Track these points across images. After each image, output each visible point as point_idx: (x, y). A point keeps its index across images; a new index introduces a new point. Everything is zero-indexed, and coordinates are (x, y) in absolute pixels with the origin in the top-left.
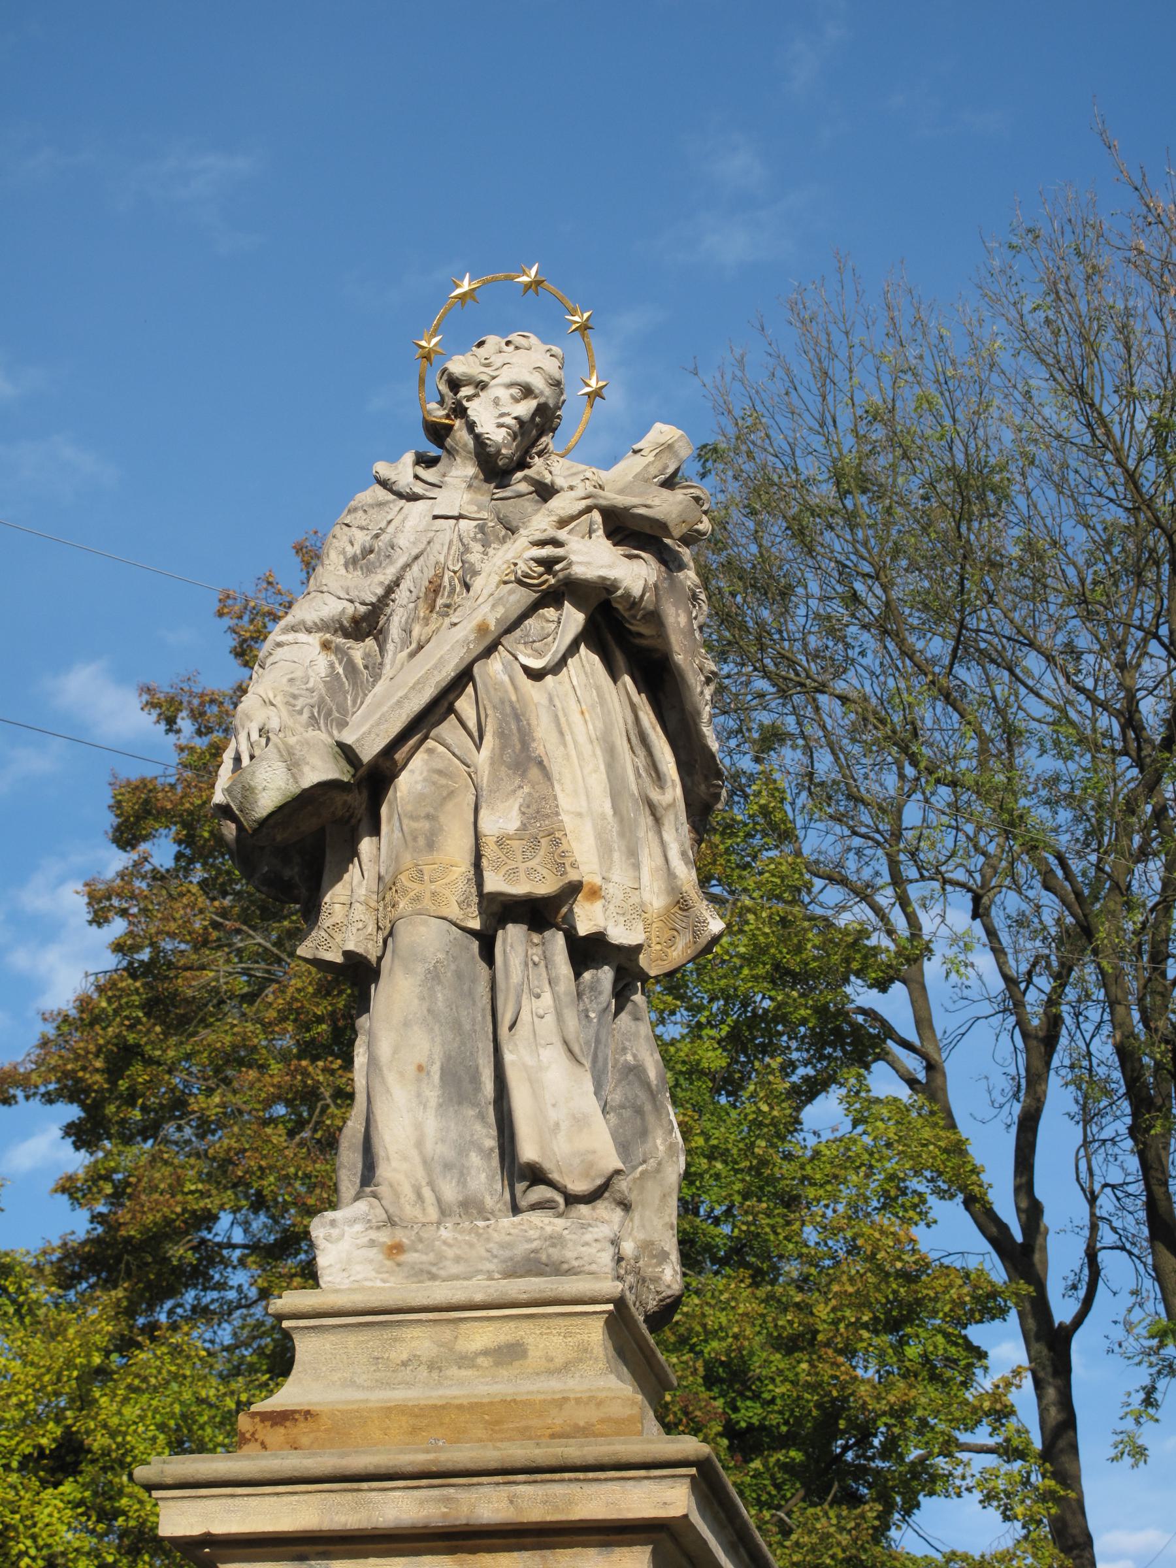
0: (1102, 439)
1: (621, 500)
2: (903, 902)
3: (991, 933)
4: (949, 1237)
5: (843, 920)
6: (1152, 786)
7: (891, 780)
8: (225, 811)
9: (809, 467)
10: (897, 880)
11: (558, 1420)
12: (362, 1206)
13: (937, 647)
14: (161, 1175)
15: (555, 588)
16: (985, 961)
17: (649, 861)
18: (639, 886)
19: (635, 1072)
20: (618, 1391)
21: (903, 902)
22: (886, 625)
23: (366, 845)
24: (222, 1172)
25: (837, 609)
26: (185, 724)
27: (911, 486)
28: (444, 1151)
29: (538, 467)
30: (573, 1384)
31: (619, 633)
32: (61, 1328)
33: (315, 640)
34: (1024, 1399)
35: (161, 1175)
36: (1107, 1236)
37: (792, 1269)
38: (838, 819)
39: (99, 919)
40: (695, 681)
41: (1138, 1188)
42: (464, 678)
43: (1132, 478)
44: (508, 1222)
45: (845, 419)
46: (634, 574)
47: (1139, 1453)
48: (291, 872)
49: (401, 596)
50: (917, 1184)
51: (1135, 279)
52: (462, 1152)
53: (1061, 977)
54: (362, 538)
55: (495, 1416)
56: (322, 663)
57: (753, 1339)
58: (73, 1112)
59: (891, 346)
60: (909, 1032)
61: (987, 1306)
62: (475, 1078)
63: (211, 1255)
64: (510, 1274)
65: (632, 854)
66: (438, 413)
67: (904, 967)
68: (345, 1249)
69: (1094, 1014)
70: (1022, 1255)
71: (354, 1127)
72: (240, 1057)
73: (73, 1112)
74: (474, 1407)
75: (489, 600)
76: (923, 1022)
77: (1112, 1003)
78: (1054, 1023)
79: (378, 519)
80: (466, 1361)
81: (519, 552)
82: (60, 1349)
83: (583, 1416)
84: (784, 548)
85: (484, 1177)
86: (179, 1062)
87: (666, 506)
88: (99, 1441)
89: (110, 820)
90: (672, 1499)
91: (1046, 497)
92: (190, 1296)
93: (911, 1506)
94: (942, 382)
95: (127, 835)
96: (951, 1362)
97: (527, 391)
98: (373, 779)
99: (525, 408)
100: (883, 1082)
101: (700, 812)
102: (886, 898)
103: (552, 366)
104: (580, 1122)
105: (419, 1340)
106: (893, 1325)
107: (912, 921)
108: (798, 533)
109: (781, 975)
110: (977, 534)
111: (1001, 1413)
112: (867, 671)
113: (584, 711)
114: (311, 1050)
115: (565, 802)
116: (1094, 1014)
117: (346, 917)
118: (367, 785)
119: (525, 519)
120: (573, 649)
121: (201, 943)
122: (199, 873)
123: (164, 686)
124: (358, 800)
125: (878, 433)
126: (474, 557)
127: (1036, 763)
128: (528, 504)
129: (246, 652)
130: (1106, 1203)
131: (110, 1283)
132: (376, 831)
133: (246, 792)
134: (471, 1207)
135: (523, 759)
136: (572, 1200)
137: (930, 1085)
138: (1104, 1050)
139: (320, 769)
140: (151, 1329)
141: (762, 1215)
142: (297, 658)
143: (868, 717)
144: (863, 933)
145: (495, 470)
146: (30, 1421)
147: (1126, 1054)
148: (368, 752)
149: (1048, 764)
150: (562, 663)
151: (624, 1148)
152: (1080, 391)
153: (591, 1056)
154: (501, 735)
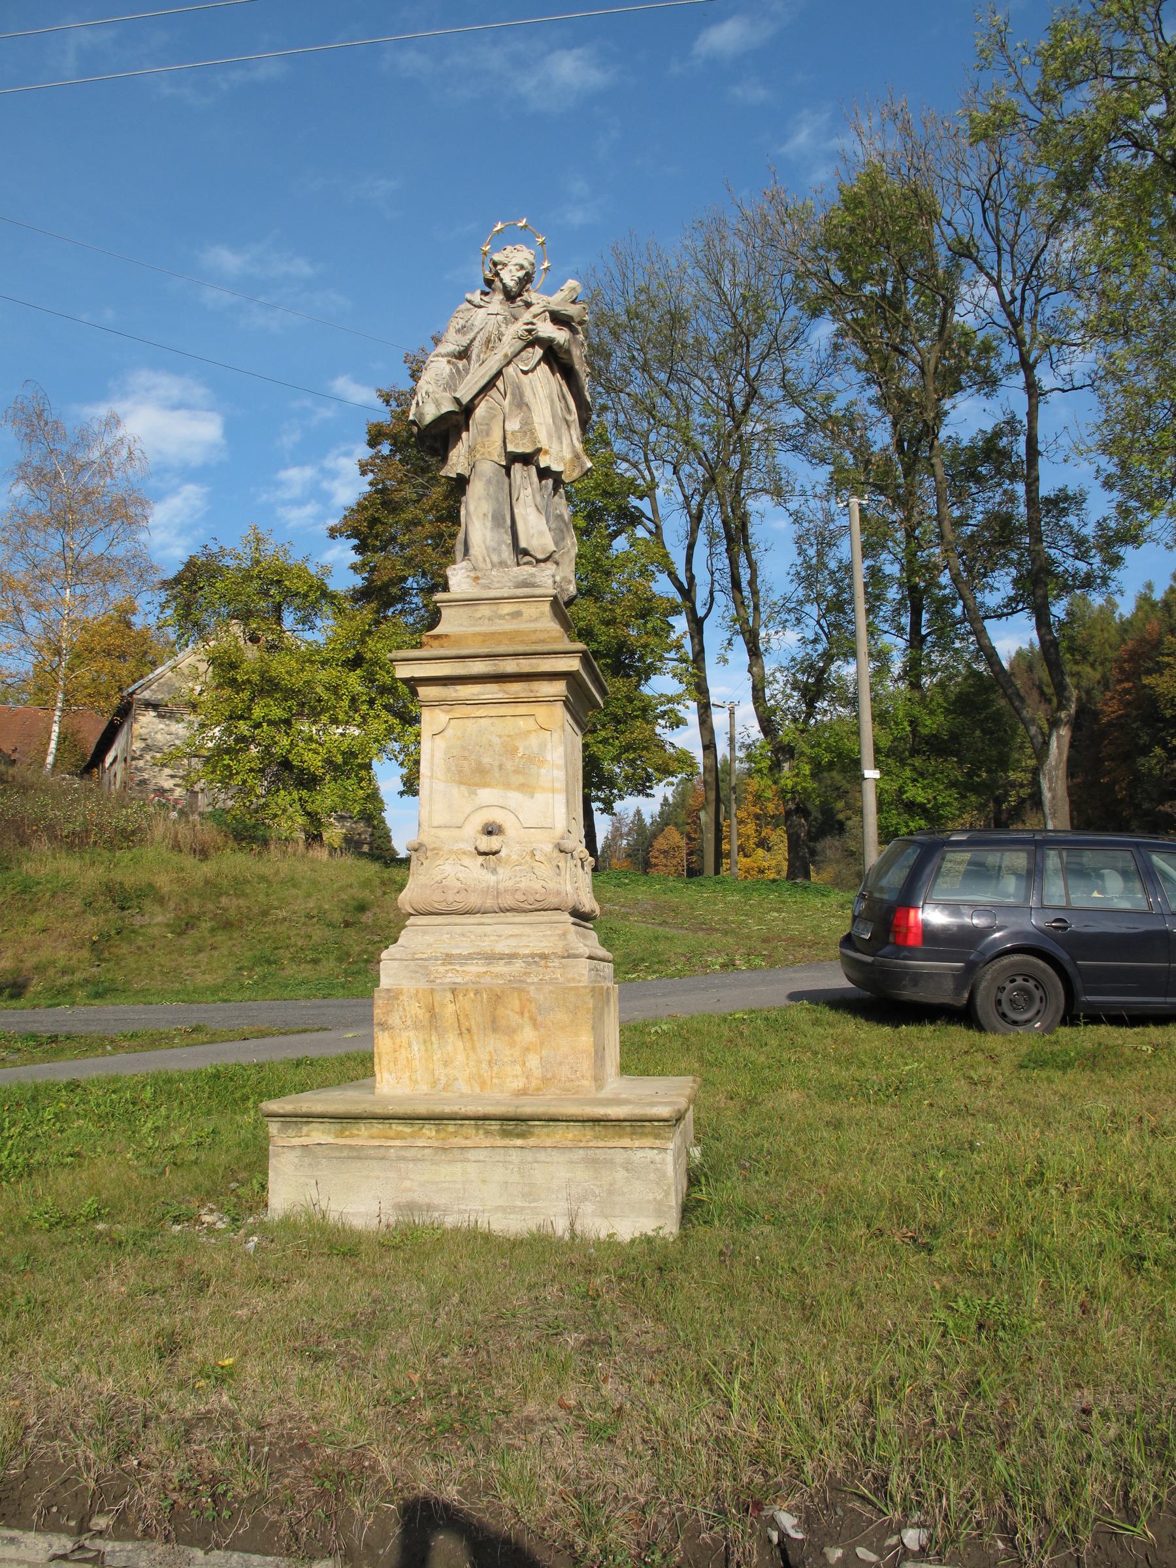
0: (725, 302)
1: (556, 308)
2: (649, 469)
3: (679, 479)
4: (662, 586)
5: (628, 475)
6: (737, 427)
7: (645, 424)
8: (413, 422)
9: (618, 309)
10: (647, 460)
11: (534, 637)
12: (464, 563)
13: (663, 377)
14: (388, 564)
15: (532, 341)
16: (676, 488)
17: (566, 441)
18: (562, 451)
19: (561, 516)
20: (555, 627)
21: (649, 469)
22: (645, 368)
23: (464, 435)
24: (408, 562)
25: (626, 362)
26: (393, 403)
27: (655, 316)
28: (493, 544)
29: (526, 296)
30: (538, 625)
31: (555, 358)
32: (354, 617)
33: (445, 360)
34: (687, 642)
35: (388, 564)
36: (717, 587)
37: (608, 597)
38: (627, 438)
39: (364, 473)
40: (583, 376)
41: (728, 570)
42: (499, 373)
43: (734, 315)
44: (516, 569)
45: (631, 293)
46: (561, 336)
47: (726, 661)
48: (438, 445)
49: (476, 343)
50: (651, 568)
51: (737, 241)
52: (499, 544)
53: (704, 496)
54: (462, 322)
55: (512, 636)
56: (447, 369)
57: (595, 621)
58: (356, 542)
59: (649, 264)
60: (650, 514)
61: (675, 610)
62: (504, 519)
63: (406, 592)
64: (517, 587)
65: (560, 438)
66: (489, 276)
67: (648, 492)
68: (459, 578)
69: (715, 509)
70: (687, 593)
71: (461, 536)
72: (416, 522)
73: (356, 542)
74: (505, 633)
75: (508, 345)
76: (655, 511)
77: (721, 505)
78: (701, 512)
79: (467, 315)
80: (501, 617)
81: (519, 327)
82: (354, 624)
83: (542, 636)
84: (608, 339)
85: (507, 553)
86: (393, 525)
87: (572, 310)
88: (368, 655)
89: (367, 437)
90: (573, 664)
91: (703, 322)
92: (399, 607)
93: (647, 679)
94: (667, 278)
95: (373, 443)
96: (662, 629)
97: (522, 267)
98: (466, 411)
99: (521, 274)
100: (640, 532)
101: (584, 423)
102: (642, 467)
103: (531, 258)
104: (541, 534)
105: (485, 610)
106: (643, 617)
107: (651, 473)
108: (614, 333)
109: (605, 494)
110: (677, 334)
111: (679, 647)
112: (638, 384)
113: (543, 385)
114: (440, 519)
115: (536, 419)
116: (715, 509)
117: (457, 461)
118: (466, 411)
119: (521, 315)
120: (538, 363)
121: (400, 482)
122: (398, 457)
123: (386, 388)
124: (461, 418)
125: (643, 297)
126: (503, 329)
127: (697, 418)
128: (522, 310)
129: (415, 376)
130: (717, 576)
131: (369, 602)
132: (468, 430)
133: (421, 415)
134: (503, 564)
135: (521, 403)
136: (538, 561)
137: (657, 533)
138: (718, 522)
139: (448, 407)
140: (385, 618)
141: (599, 578)
142: (438, 367)
143: (637, 401)
144: (635, 479)
145: (510, 296)
146: (344, 649)
147: (725, 523)
148: (465, 401)
149: (702, 420)
150: (533, 370)
151: (556, 544)
152: (717, 283)
153: (545, 510)
154: (513, 394)
